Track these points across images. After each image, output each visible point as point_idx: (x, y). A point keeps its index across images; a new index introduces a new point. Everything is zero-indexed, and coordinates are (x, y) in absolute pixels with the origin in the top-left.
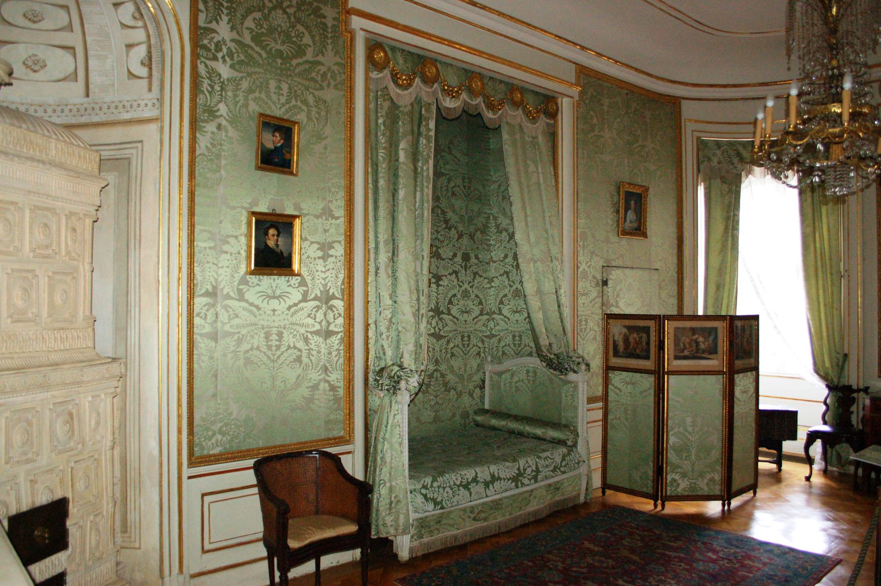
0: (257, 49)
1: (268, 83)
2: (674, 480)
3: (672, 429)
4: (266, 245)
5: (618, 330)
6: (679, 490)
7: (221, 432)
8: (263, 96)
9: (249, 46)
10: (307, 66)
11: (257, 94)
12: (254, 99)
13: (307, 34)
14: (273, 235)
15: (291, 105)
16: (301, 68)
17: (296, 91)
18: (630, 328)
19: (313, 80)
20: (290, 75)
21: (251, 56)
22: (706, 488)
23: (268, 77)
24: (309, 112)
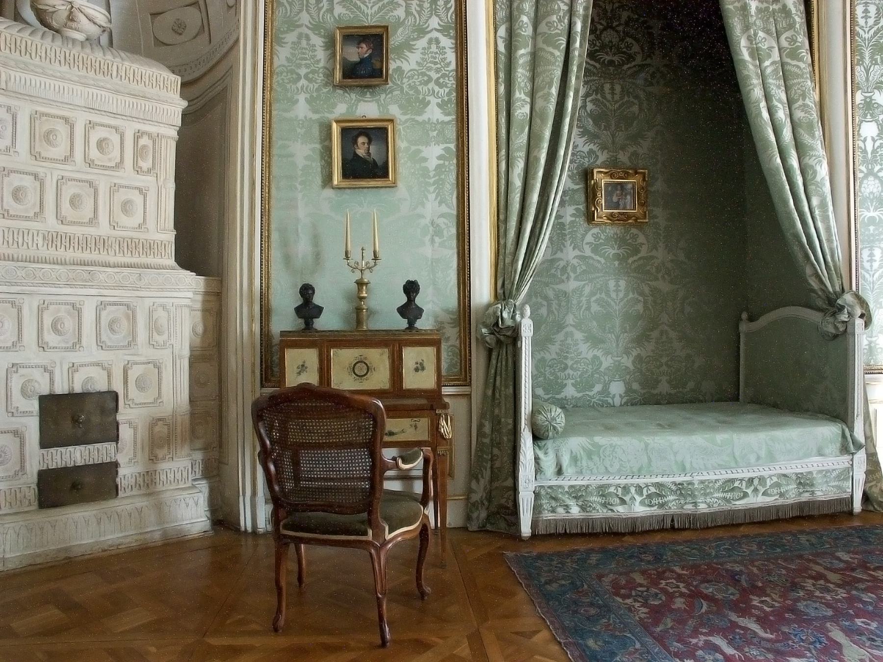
1: (602, 87)
4: (356, 155)
8: (599, 97)
9: (590, 257)
10: (641, 262)
11: (598, 296)
12: (591, 101)
13: (640, 234)
14: (364, 143)
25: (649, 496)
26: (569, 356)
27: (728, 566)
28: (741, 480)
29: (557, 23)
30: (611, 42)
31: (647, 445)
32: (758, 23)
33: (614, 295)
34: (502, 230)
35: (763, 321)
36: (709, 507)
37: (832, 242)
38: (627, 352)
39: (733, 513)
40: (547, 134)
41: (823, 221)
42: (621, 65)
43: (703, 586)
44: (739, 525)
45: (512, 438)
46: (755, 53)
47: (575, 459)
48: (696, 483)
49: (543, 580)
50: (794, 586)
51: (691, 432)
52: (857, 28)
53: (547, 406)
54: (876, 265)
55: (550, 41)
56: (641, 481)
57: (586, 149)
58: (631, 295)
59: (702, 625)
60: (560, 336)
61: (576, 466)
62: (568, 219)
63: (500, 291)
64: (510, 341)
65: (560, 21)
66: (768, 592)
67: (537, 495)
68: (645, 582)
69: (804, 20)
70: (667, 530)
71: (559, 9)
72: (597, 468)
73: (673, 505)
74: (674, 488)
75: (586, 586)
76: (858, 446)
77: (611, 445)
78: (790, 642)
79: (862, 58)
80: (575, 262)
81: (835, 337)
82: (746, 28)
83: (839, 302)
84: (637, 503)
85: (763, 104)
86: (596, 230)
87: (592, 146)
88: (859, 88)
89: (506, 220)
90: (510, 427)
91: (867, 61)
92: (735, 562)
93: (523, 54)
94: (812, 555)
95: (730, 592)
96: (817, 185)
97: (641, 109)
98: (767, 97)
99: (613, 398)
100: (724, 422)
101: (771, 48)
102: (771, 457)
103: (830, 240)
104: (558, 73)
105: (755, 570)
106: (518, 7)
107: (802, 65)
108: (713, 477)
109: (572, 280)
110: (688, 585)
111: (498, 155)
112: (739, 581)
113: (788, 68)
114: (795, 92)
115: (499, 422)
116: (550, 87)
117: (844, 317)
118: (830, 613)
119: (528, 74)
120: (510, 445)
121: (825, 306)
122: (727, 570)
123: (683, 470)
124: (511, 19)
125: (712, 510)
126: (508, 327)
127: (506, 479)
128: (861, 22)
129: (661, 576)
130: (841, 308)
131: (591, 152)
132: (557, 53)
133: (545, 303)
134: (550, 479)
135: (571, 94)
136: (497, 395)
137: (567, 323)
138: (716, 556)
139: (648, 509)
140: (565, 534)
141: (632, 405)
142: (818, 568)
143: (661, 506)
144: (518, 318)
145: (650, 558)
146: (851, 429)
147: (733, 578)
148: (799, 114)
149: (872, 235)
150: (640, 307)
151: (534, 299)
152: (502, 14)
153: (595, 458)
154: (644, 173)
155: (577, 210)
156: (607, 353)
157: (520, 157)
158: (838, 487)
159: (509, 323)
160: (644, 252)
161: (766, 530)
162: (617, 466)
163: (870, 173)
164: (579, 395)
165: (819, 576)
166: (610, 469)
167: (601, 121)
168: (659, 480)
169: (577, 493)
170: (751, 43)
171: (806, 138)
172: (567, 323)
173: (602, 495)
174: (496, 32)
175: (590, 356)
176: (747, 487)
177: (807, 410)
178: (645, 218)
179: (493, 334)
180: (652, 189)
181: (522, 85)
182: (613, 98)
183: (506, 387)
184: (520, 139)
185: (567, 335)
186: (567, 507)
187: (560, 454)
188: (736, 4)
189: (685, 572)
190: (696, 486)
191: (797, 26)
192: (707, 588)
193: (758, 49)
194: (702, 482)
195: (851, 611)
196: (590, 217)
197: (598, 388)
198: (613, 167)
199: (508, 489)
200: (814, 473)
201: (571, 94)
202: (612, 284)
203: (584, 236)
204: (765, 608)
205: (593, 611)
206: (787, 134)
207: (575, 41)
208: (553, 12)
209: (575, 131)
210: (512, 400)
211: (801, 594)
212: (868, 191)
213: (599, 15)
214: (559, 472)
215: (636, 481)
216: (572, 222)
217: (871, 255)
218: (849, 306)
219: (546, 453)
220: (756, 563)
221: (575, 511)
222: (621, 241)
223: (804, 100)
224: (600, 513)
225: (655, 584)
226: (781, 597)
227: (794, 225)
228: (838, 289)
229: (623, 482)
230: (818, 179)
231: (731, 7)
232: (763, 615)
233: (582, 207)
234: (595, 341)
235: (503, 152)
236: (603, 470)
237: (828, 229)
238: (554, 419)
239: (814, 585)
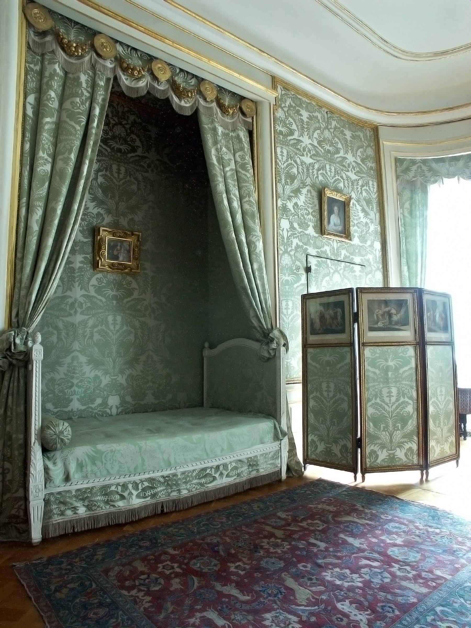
1: (111, 166)
2: (373, 452)
3: (369, 400)
5: (314, 307)
6: (379, 461)
11: (99, 328)
12: (101, 176)
13: (138, 140)
15: (127, 180)
17: (290, 155)
18: (327, 306)
22: (404, 459)
25: (144, 490)
26: (75, 375)
27: (208, 540)
28: (211, 468)
29: (80, 104)
30: (120, 134)
31: (140, 448)
32: (223, 141)
33: (112, 327)
34: (18, 267)
35: (221, 347)
36: (189, 491)
37: (266, 295)
38: (122, 372)
39: (206, 493)
40: (65, 190)
41: (260, 280)
42: (125, 153)
43: (192, 562)
44: (211, 502)
45: (22, 451)
46: (220, 160)
47: (80, 466)
48: (179, 474)
49: (53, 588)
50: (257, 548)
51: (174, 434)
52: (278, 160)
53: (56, 421)
54: (290, 311)
55: (72, 116)
56: (137, 478)
57: (95, 211)
58: (125, 328)
59: (196, 602)
60: (68, 360)
61: (82, 471)
62: (77, 265)
63: (14, 320)
64: (21, 364)
65: (83, 103)
66: (240, 557)
67: (47, 502)
68: (145, 569)
69: (249, 147)
70: (158, 514)
71: (82, 94)
72: (100, 471)
73: (163, 494)
74: (162, 480)
75: (94, 586)
76: (284, 434)
77: (112, 451)
78: (262, 600)
79: (281, 180)
80: (81, 300)
81: (269, 359)
82: (216, 143)
83: (271, 335)
84: (134, 497)
85: (224, 195)
86: (100, 275)
87: (99, 210)
88: (279, 197)
89: (23, 258)
90: (21, 442)
91: (283, 181)
92: (212, 535)
93: (48, 122)
94: (262, 518)
95: (213, 564)
96: (256, 254)
97: (139, 189)
98: (228, 192)
99: (111, 409)
100: (195, 424)
101: (230, 160)
102: (231, 449)
103: (264, 293)
104: (77, 143)
105: (228, 540)
106: (48, 82)
107: (249, 175)
108: (191, 468)
109: (78, 314)
110: (180, 564)
111: (19, 202)
112: (218, 552)
113: (240, 175)
114: (244, 192)
115: (10, 438)
116: (70, 153)
117: (274, 346)
118: (282, 564)
119: (51, 139)
120: (21, 458)
121: (261, 338)
122: (208, 544)
123: (169, 465)
124: (40, 92)
125: (191, 494)
126: (21, 352)
127: (17, 491)
128: (280, 157)
129: (158, 560)
130: (272, 340)
131: (99, 214)
132: (78, 128)
133: (55, 332)
134: (59, 485)
135: (87, 162)
136: (9, 413)
137: (74, 348)
138: (199, 533)
139: (143, 500)
140: (72, 533)
141: (126, 413)
142: (268, 528)
143: (153, 496)
144: (30, 344)
145: (148, 544)
146: (280, 423)
147: (213, 551)
148: (246, 206)
149: (287, 291)
150: (132, 337)
151: (46, 329)
152: (32, 85)
153: (98, 463)
154: (139, 236)
155: (85, 258)
156: (106, 373)
157: (39, 206)
158: (273, 464)
159: (22, 348)
160: (136, 295)
161: (229, 504)
162: (116, 468)
163: (286, 252)
164: (83, 408)
165: (271, 535)
166: (111, 471)
167: (106, 192)
168: (152, 475)
169: (83, 495)
170: (218, 154)
171: (251, 223)
172: (74, 348)
173: (106, 494)
174: (25, 98)
175: (92, 375)
176: (215, 473)
177: (250, 411)
178: (138, 269)
179: (5, 357)
180: (143, 248)
181: (46, 146)
182: (119, 176)
183: (18, 405)
184: (41, 191)
185: (73, 359)
186: (75, 509)
187: (67, 462)
188: (209, 126)
189: (176, 552)
190: (179, 477)
191: (246, 150)
192: (195, 564)
193: (222, 158)
194: (183, 473)
195: (294, 559)
196: (95, 265)
197: (99, 401)
198: (115, 227)
199: (17, 499)
200: (259, 456)
201: (87, 162)
202: (110, 318)
203: (90, 279)
204: (240, 572)
205: (102, 612)
206: (239, 217)
207: (93, 121)
208: (76, 95)
209: (87, 195)
210: (22, 417)
211: (262, 553)
212: (285, 263)
213: (112, 112)
214: (67, 479)
215: (133, 478)
216: (80, 268)
217: (287, 305)
218: (277, 338)
219: (54, 463)
220: (228, 533)
221: (82, 511)
222: (119, 286)
223: (249, 197)
224: (105, 509)
225: (154, 569)
226: (248, 560)
227: (243, 281)
228: (269, 327)
229: (122, 480)
230: (258, 251)
231: (206, 126)
232: (239, 579)
233: (89, 256)
234: (95, 363)
235: (24, 200)
236: (105, 472)
237: (263, 286)
238: (62, 432)
239: (268, 543)
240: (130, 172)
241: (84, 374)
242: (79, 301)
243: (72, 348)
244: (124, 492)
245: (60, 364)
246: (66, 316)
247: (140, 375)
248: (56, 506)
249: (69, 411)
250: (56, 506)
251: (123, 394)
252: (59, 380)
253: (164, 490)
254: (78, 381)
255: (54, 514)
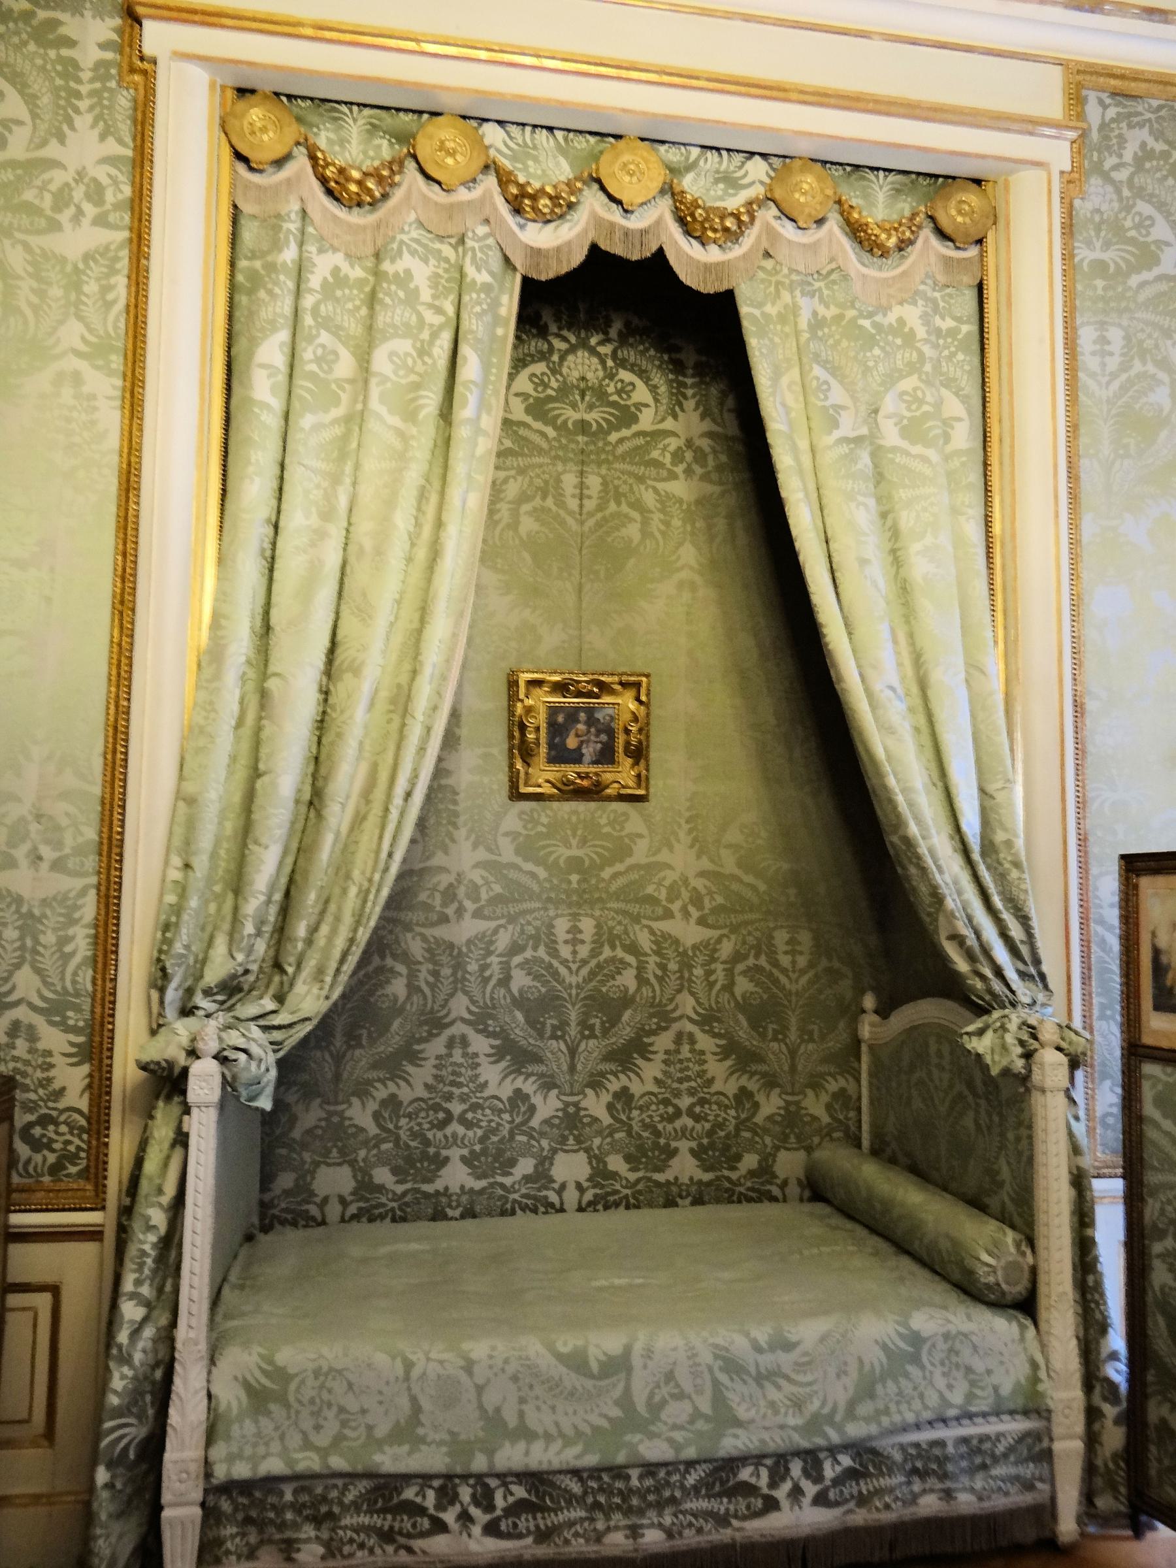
0: (537, 425)
1: (558, 481)
7: (690, 1113)
10: (641, 441)
11: (537, 502)
15: (1132, 373)
16: (627, 446)
17: (1141, 342)
19: (657, 464)
20: (1127, 309)
21: (525, 439)
23: (560, 468)
24: (645, 522)
30: (583, 379)
36: (670, 1535)
80: (476, 876)
109: (467, 916)
240: (616, 488)
241: (485, 1085)
242: (471, 881)
243: (447, 1015)
244: (444, 1509)
245: (415, 1058)
246: (433, 925)
247: (652, 1093)
248: (235, 1530)
249: (437, 1193)
250: (235, 1530)
251: (599, 1148)
252: (412, 1102)
253: (582, 1520)
254: (464, 1107)
255: (228, 1553)
